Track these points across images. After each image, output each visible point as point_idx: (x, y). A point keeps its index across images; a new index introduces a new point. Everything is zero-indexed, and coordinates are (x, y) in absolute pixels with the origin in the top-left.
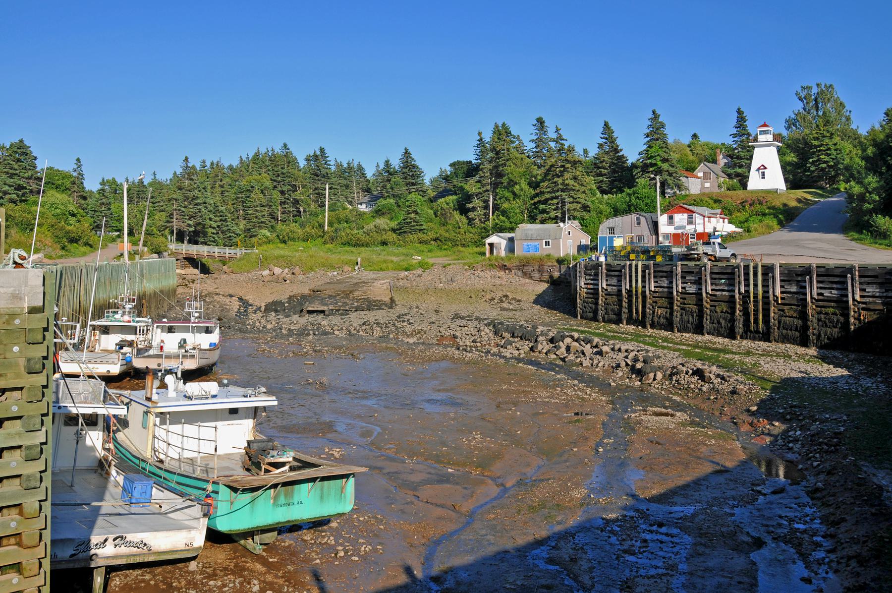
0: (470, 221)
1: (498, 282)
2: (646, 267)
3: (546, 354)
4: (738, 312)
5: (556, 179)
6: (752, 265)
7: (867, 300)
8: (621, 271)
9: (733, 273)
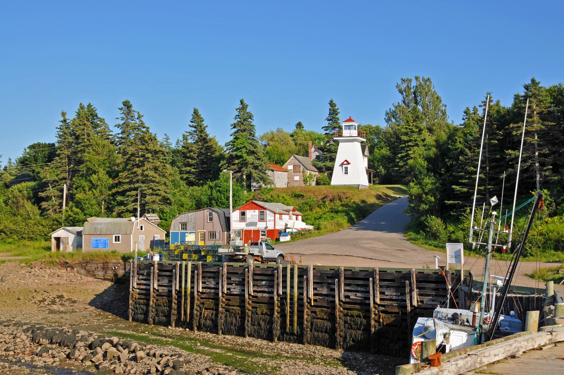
0: (43, 211)
1: (56, 280)
2: (195, 267)
3: (82, 361)
4: (276, 313)
5: (135, 169)
6: (289, 267)
7: (385, 303)
8: (171, 271)
9: (273, 275)
